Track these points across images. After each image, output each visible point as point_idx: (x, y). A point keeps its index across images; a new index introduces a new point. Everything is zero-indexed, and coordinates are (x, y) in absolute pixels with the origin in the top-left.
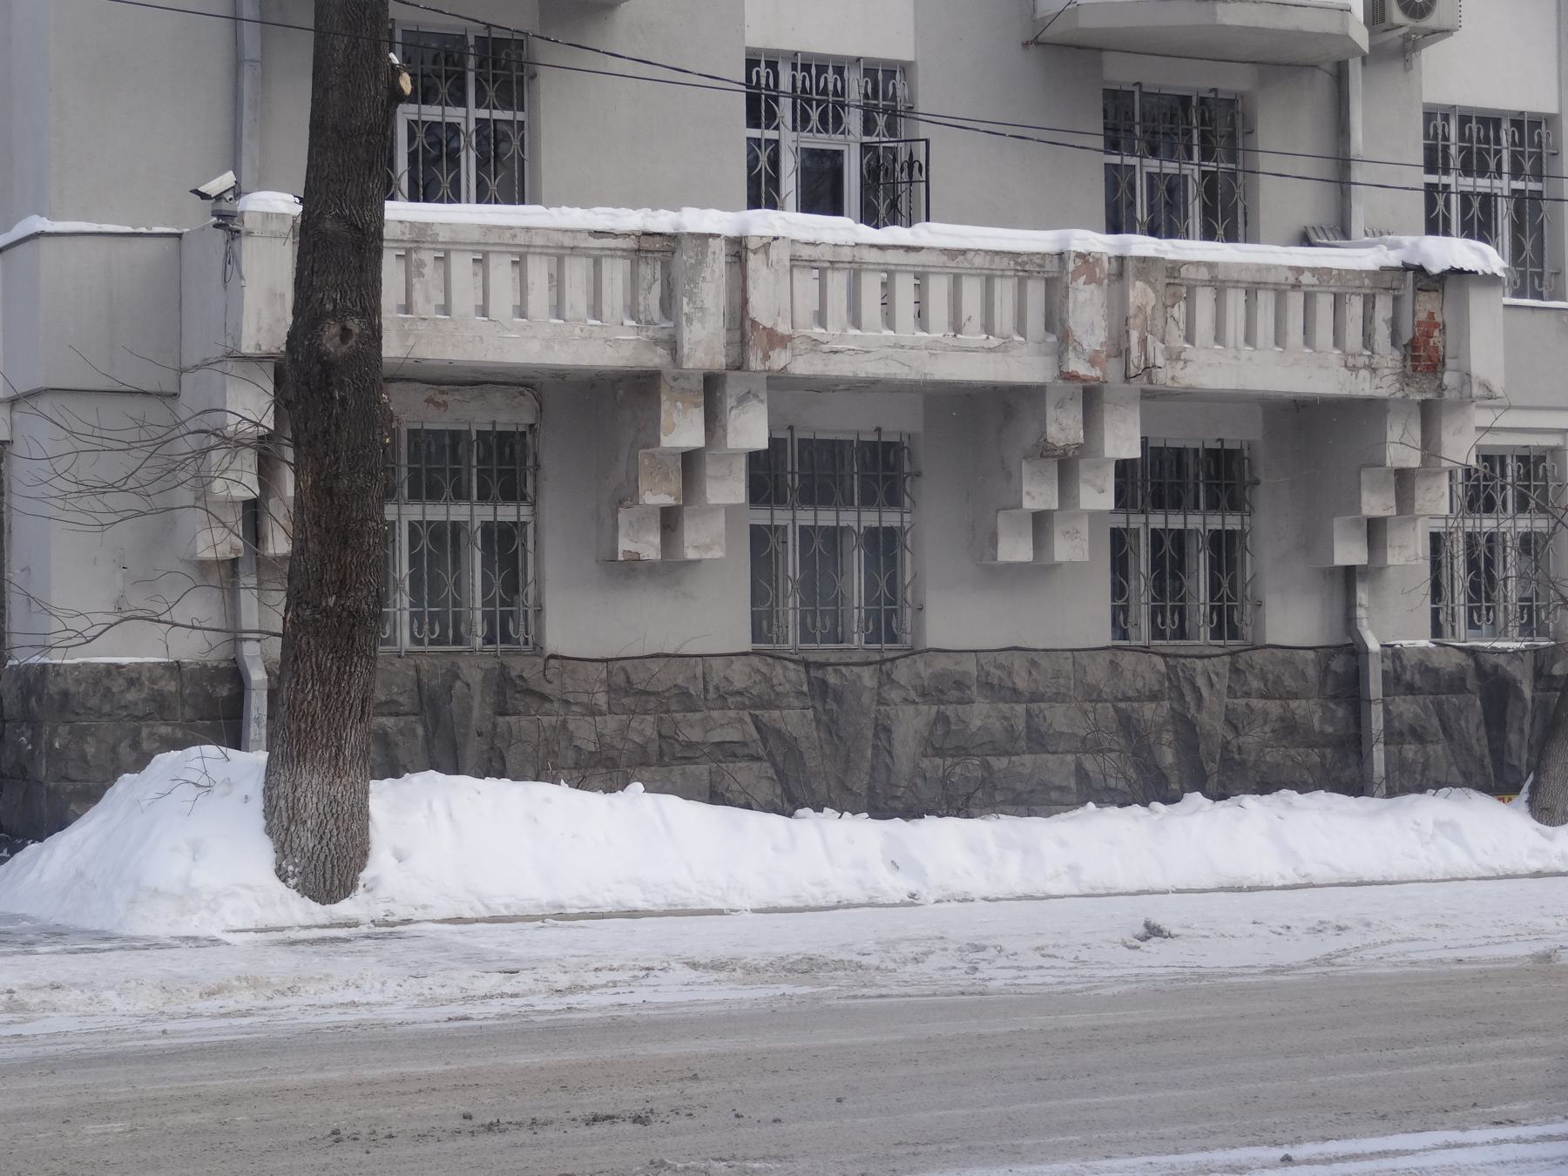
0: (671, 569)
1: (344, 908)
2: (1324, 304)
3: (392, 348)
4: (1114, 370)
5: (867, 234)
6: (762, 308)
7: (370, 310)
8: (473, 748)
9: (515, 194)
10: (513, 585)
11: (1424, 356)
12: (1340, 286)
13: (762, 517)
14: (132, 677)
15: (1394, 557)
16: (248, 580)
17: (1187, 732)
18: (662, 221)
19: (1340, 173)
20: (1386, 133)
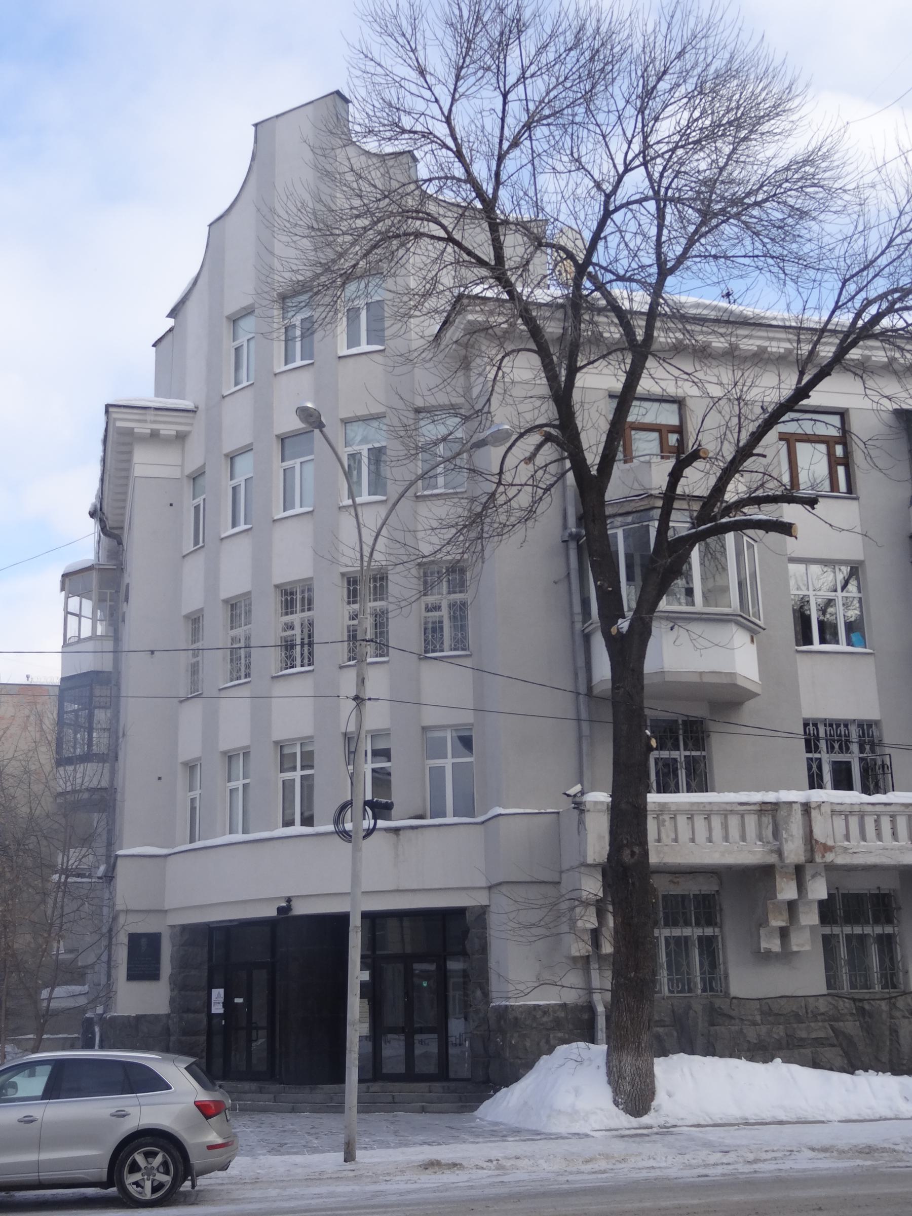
0: (786, 956)
1: (646, 1120)
3: (653, 859)
5: (866, 798)
6: (819, 833)
7: (643, 843)
10: (713, 965)
13: (827, 930)
16: (594, 965)
18: (770, 797)
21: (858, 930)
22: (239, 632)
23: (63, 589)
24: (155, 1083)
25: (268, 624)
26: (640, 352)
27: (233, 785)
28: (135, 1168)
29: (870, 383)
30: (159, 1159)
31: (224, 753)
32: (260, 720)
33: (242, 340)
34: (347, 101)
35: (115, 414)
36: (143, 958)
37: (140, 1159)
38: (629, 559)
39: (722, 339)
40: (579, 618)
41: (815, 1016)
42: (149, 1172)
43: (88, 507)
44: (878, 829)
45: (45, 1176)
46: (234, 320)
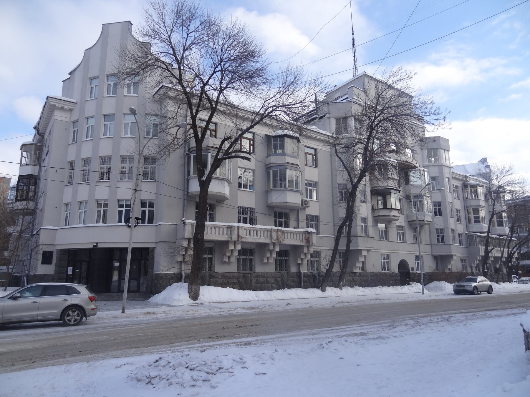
0: (229, 263)
1: (197, 302)
2: (298, 235)
3: (205, 238)
4: (277, 241)
5: (251, 226)
6: (241, 234)
7: (203, 234)
8: (207, 283)
9: (213, 221)
10: (211, 264)
11: (308, 241)
12: (299, 233)
13: (238, 257)
14: (169, 274)
15: (304, 262)
16: (183, 263)
17: (283, 282)
18: (230, 224)
19: (298, 221)
20: (302, 217)
21: (245, 257)
22: (87, 168)
23: (21, 149)
24: (77, 292)
25: (96, 166)
26: (213, 110)
27: (81, 211)
28: (69, 315)
29: (155, 82)
30: (76, 313)
31: (79, 202)
32: (92, 193)
33: (94, 85)
34: (132, 25)
35: (50, 99)
36: (47, 257)
37: (70, 313)
38: (201, 161)
39: (233, 111)
40: (186, 175)
41: (234, 277)
42: (73, 316)
43: (34, 126)
44: (253, 234)
45: (39, 318)
46: (91, 79)
